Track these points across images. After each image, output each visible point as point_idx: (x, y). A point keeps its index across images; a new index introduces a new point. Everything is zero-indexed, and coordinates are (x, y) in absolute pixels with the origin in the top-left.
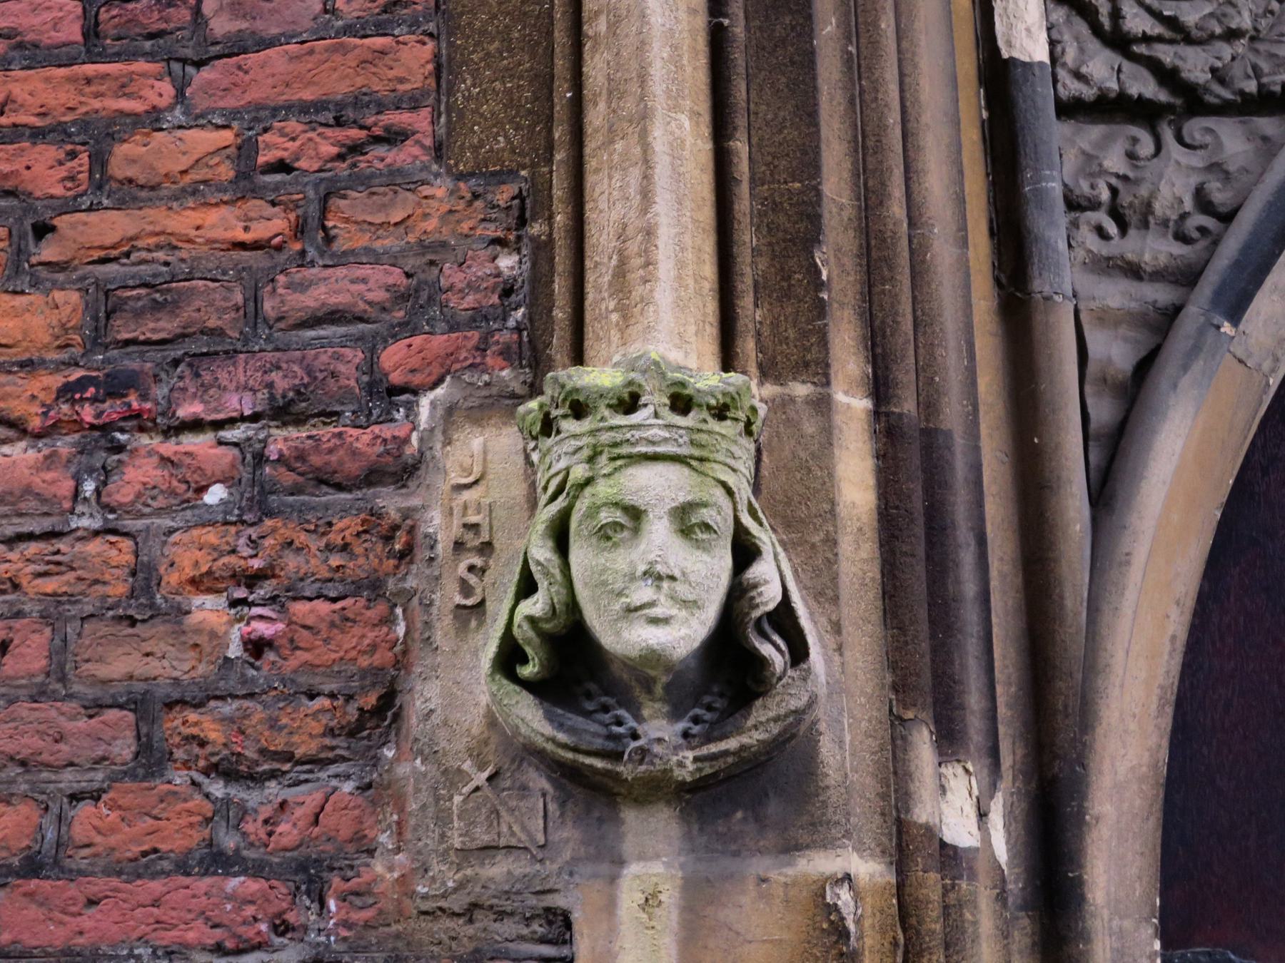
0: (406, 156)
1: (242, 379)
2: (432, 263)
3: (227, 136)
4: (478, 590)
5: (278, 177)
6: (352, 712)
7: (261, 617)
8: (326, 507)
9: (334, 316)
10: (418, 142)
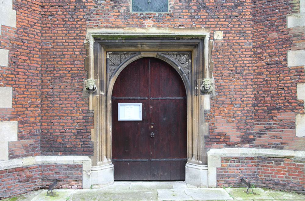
0: (83, 69)
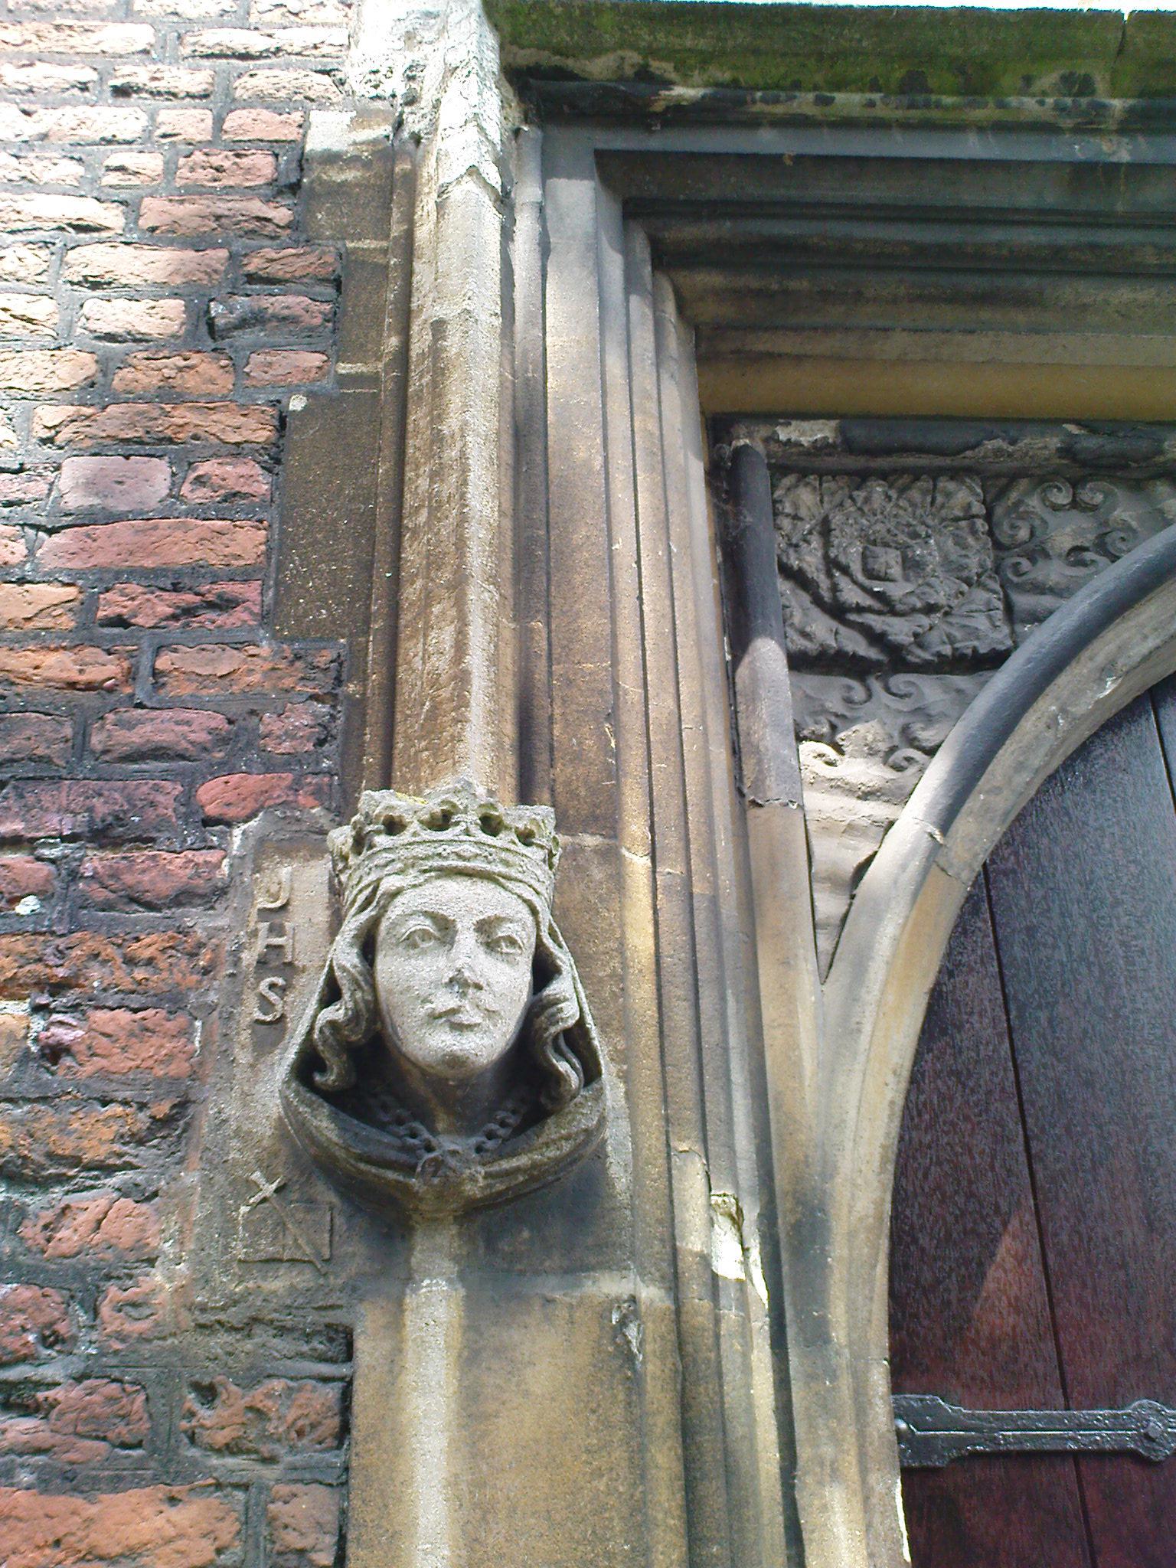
1: (65, 802)
2: (253, 712)
3: (72, 592)
4: (279, 1007)
5: (116, 630)
6: (142, 1120)
7: (61, 1023)
8: (135, 923)
9: (158, 753)
10: (247, 609)
